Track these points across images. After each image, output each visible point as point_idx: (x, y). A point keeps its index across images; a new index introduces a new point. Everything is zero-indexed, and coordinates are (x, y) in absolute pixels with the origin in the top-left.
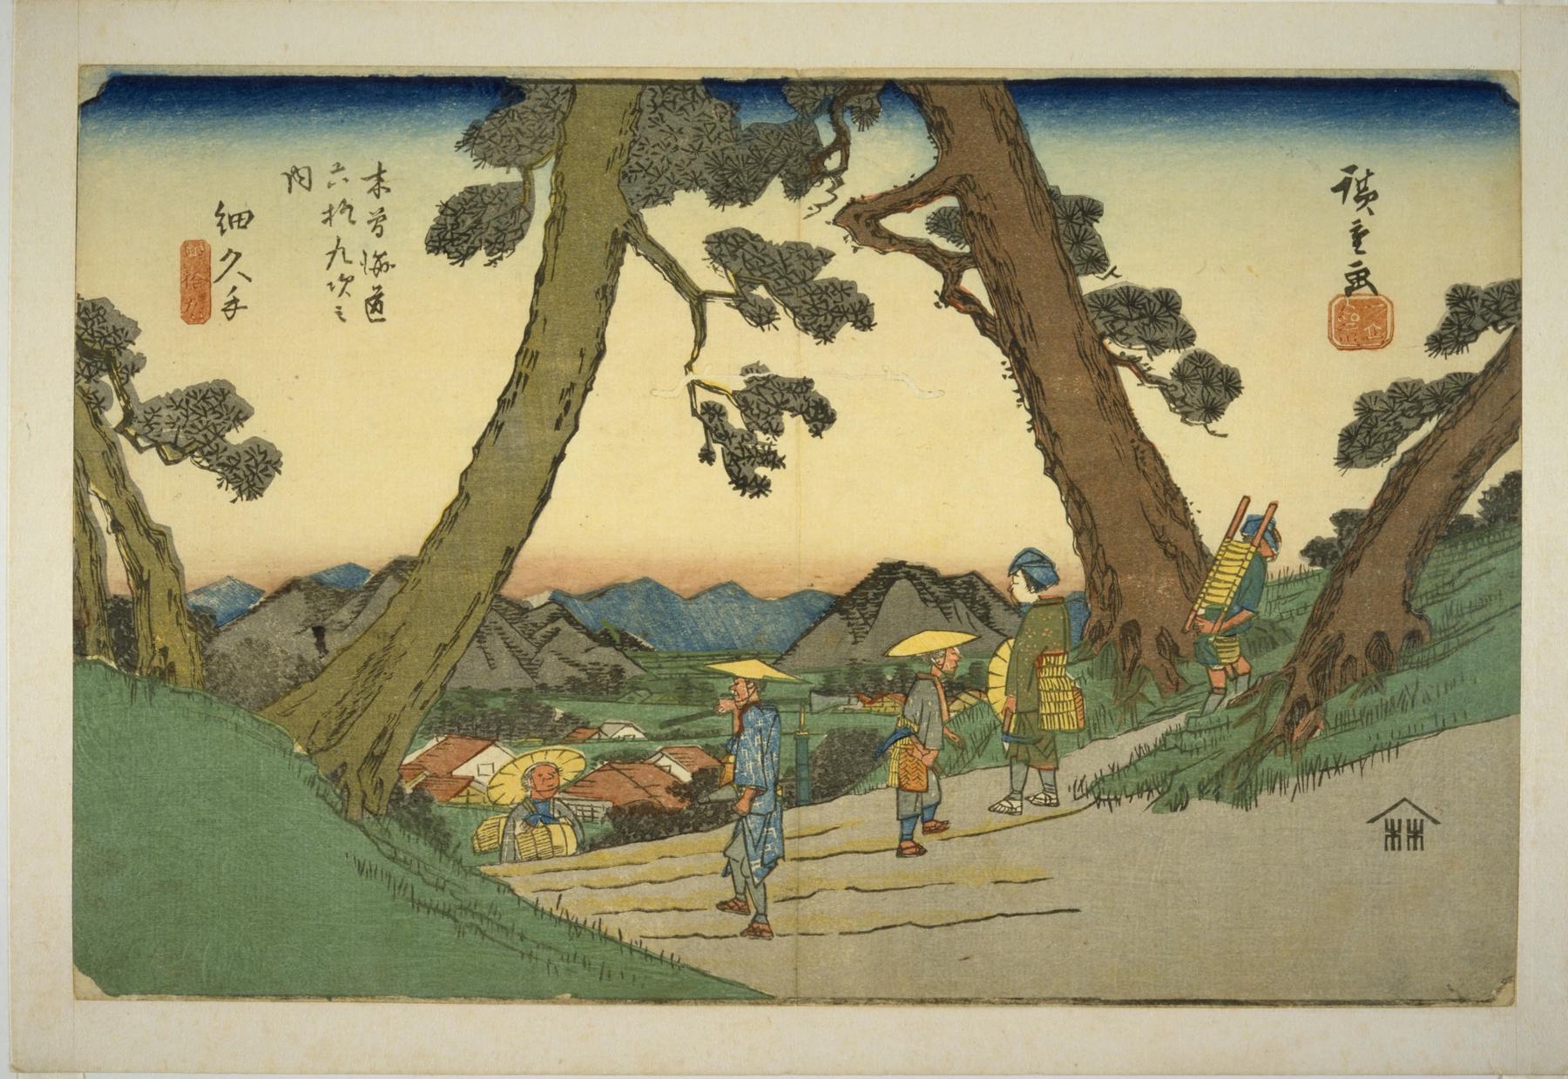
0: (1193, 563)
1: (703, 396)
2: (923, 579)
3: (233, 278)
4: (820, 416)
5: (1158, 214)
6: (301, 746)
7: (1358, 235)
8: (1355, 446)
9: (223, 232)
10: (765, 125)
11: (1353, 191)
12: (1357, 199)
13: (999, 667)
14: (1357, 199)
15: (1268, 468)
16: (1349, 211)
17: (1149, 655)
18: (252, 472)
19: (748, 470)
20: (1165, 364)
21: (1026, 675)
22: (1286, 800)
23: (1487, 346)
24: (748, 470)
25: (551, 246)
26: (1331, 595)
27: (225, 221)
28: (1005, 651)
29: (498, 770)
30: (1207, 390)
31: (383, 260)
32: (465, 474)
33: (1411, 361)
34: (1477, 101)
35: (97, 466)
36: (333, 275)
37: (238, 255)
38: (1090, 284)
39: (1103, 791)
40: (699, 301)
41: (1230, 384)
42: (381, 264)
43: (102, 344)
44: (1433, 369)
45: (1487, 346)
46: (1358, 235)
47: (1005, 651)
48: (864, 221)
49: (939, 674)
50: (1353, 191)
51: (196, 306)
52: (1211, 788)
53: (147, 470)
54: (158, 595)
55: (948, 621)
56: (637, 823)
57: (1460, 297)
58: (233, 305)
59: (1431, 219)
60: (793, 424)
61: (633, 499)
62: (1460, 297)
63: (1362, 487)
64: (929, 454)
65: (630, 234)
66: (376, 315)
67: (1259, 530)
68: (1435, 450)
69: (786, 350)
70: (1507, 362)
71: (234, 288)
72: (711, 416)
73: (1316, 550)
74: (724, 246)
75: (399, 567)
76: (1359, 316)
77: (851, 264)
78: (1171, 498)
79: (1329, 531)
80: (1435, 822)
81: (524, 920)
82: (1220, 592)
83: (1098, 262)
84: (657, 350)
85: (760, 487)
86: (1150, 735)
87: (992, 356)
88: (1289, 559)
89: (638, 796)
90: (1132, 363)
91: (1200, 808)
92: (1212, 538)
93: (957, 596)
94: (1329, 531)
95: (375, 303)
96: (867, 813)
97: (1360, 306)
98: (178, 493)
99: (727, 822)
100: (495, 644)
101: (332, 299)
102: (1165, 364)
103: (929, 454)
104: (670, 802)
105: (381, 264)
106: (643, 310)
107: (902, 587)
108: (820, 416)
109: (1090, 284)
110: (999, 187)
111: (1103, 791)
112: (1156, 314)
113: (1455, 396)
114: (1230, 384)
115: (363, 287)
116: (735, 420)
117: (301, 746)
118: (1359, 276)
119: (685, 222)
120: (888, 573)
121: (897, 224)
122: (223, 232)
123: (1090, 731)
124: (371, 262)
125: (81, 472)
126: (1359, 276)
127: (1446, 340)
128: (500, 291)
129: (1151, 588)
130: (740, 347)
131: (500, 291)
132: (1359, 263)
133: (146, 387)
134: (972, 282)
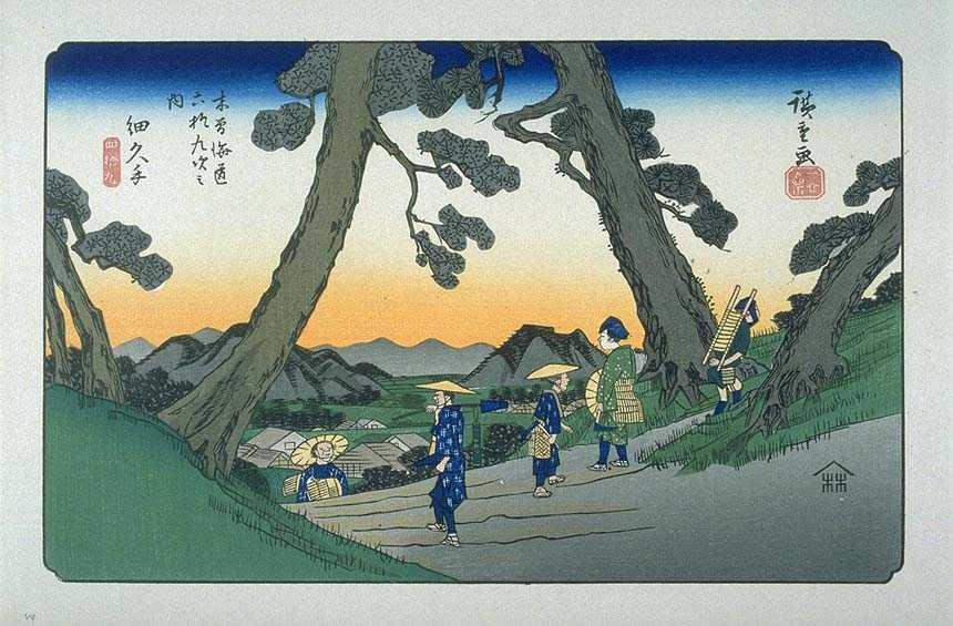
0: (705, 329)
1: (418, 228)
2: (546, 333)
3: (137, 160)
4: (486, 240)
5: (688, 128)
6: (163, 431)
7: (803, 130)
8: (799, 262)
9: (131, 133)
10: (456, 68)
11: (800, 106)
12: (802, 110)
13: (592, 388)
14: (802, 110)
15: (751, 271)
16: (799, 117)
17: (683, 379)
18: (153, 272)
19: (445, 268)
20: (689, 210)
21: (607, 391)
22: (766, 462)
23: (877, 199)
24: (445, 268)
25: (327, 137)
26: (788, 344)
27: (133, 128)
28: (596, 377)
29: (300, 449)
30: (716, 224)
31: (224, 148)
32: (276, 272)
33: (831, 206)
34: (866, 61)
35: (56, 271)
36: (196, 157)
37: (140, 146)
38: (646, 164)
39: (655, 460)
40: (412, 169)
41: (729, 221)
42: (223, 150)
43: (62, 199)
44: (845, 211)
45: (877, 199)
46: (803, 130)
47: (596, 377)
48: (511, 126)
49: (558, 391)
50: (800, 106)
51: (112, 176)
52: (721, 457)
53: (90, 274)
54: (96, 349)
55: (567, 359)
56: (379, 479)
57: (866, 170)
58: (138, 176)
59: (848, 129)
60: (471, 243)
61: (377, 289)
62: (866, 170)
63: (807, 282)
64: (549, 247)
65: (373, 135)
66: (221, 180)
67: (747, 306)
68: (856, 251)
69: (467, 200)
70: (893, 208)
71: (138, 166)
72: (421, 239)
73: (781, 318)
74: (426, 141)
75: (238, 330)
76: (804, 177)
77: (502, 146)
78: (692, 285)
79: (788, 307)
80: (852, 474)
81: (330, 543)
82: (722, 342)
83: (651, 148)
84: (390, 203)
85: (453, 282)
86: (681, 426)
87: (590, 207)
88: (765, 325)
89: (380, 463)
90: (671, 209)
91: (714, 469)
92: (719, 311)
93: (571, 346)
94: (788, 307)
95: (221, 171)
96: (515, 471)
97: (805, 173)
98: (105, 284)
99: (429, 477)
100: (298, 373)
101: (197, 171)
102: (689, 210)
103: (549, 247)
104: (400, 467)
105: (223, 150)
106: (381, 174)
107: (537, 345)
108: (486, 240)
109: (646, 164)
110: (594, 97)
111: (655, 460)
112: (685, 181)
113: (862, 226)
114: (729, 221)
115: (213, 163)
116: (435, 239)
117: (163, 431)
118: (804, 155)
119: (405, 125)
120: (528, 333)
121: (529, 125)
122: (131, 133)
123: (650, 423)
124: (217, 150)
125: (49, 272)
126: (804, 155)
127: (855, 195)
128: (297, 167)
129: (682, 351)
130: (435, 195)
131: (297, 167)
132: (804, 147)
133: (89, 227)
134: (577, 160)
